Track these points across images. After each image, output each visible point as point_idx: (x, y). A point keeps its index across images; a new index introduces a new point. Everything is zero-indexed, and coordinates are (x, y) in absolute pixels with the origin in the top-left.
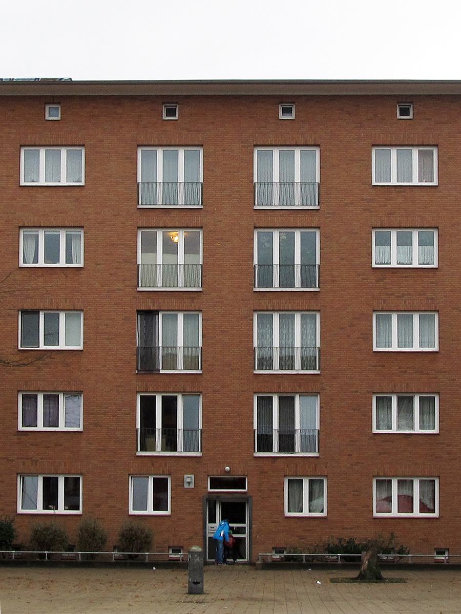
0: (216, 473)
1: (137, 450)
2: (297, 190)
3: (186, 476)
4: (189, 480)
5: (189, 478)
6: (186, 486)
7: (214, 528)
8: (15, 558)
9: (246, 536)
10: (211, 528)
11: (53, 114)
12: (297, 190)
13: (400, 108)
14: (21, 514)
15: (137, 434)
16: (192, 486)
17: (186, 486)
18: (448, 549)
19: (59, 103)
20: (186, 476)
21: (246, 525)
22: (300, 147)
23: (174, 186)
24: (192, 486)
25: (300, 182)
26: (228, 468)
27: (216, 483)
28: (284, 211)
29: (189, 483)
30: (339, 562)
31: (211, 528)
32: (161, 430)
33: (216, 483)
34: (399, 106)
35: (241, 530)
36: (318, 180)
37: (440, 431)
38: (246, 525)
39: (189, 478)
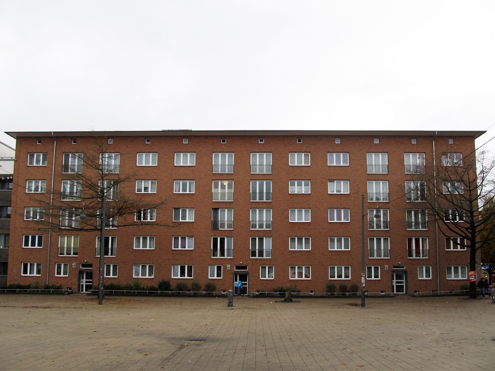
2: (227, 167)
3: (227, 265)
4: (228, 267)
5: (228, 266)
12: (227, 167)
20: (227, 265)
27: (238, 268)
29: (228, 268)
30: (278, 295)
39: (228, 266)
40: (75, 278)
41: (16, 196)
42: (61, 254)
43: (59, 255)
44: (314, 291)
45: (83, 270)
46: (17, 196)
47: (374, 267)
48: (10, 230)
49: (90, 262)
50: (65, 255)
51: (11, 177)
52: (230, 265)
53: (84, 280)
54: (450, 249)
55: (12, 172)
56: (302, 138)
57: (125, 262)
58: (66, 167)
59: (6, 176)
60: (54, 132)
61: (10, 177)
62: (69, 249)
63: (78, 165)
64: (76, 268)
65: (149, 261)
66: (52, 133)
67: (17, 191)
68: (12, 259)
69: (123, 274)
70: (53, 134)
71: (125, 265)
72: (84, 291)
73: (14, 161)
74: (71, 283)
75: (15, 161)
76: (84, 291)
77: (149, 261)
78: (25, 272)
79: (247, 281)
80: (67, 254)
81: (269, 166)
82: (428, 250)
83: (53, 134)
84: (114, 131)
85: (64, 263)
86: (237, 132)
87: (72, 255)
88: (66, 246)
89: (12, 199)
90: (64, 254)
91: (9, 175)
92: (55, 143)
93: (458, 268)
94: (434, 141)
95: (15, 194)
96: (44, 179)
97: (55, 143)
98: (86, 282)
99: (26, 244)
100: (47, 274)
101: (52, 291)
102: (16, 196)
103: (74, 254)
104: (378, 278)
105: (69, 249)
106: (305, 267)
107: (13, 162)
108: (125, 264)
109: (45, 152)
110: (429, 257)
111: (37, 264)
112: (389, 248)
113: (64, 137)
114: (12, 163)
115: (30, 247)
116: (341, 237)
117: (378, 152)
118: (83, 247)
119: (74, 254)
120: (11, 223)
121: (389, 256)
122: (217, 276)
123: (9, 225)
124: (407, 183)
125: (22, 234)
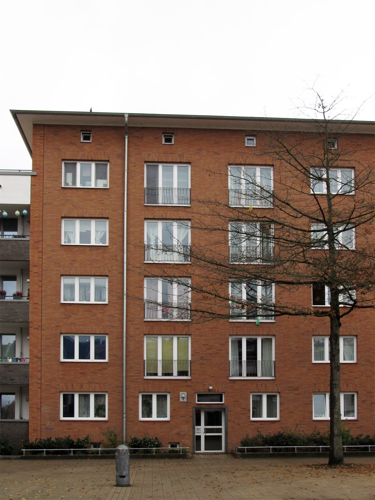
0: (202, 391)
1: (144, 375)
2: (175, 193)
3: (181, 393)
4: (183, 396)
5: (183, 394)
6: (181, 400)
7: (199, 429)
8: (322, 451)
9: (223, 434)
10: (197, 429)
11: (250, 143)
12: (175, 193)
13: (165, 138)
14: (141, 421)
15: (144, 364)
16: (185, 400)
17: (181, 400)
18: (179, 443)
19: (254, 136)
20: (181, 393)
21: (223, 427)
22: (80, 162)
23: (170, 191)
24: (185, 400)
25: (315, 193)
26: (211, 388)
27: (201, 396)
28: (180, 208)
29: (183, 398)
30: (271, 452)
31: (197, 429)
32: (246, 361)
33: (201, 396)
34: (164, 136)
35: (219, 431)
36: (190, 187)
37: (275, 359)
38: (223, 427)
39: (183, 394)
40: (187, 422)
41: (39, 252)
42: (149, 374)
43: (146, 377)
44: (179, 443)
45: (202, 406)
46: (42, 252)
47: (158, 396)
48: (30, 324)
49: (219, 389)
50: (160, 377)
51: (25, 212)
52: (186, 393)
53: (203, 427)
54: (89, 359)
55: (26, 200)
56: (173, 134)
57: (296, 389)
58: (153, 191)
59: (11, 208)
60: (131, 116)
61: (21, 211)
62: (167, 363)
63: (163, 189)
64: (187, 402)
65: (347, 385)
66: (126, 116)
67: (42, 241)
68: (39, 386)
69: (291, 412)
70: (126, 119)
71: (295, 394)
72: (203, 450)
73: (30, 177)
74: (178, 434)
75: (32, 176)
76: (203, 450)
77: (347, 385)
78: (69, 411)
79: (221, 425)
80: (164, 374)
81: (185, 191)
82: (275, 362)
83: (126, 119)
84: (286, 118)
85: (267, 392)
86: (149, 118)
87: (175, 376)
88: (160, 357)
89: (31, 258)
90: (171, 374)
91: (21, 207)
92: (126, 140)
93: (87, 397)
94: (127, 137)
95: (38, 248)
96: (105, 216)
97: (126, 140)
98: (207, 431)
99: (69, 353)
100: (123, 415)
101: (156, 452)
102: (39, 252)
103: (180, 373)
104: (104, 417)
105: (167, 363)
106: (80, 395)
107: (29, 178)
108: (297, 392)
109: (103, 159)
110: (275, 376)
111: (268, 396)
112: (274, 359)
113: (144, 128)
114: (28, 180)
115: (77, 359)
116: (240, 337)
117: (88, 160)
118: (202, 358)
119: (180, 373)
120: (31, 309)
121: (189, 375)
122: (268, 416)
123: (27, 314)
124: (179, 227)
125: (59, 332)
